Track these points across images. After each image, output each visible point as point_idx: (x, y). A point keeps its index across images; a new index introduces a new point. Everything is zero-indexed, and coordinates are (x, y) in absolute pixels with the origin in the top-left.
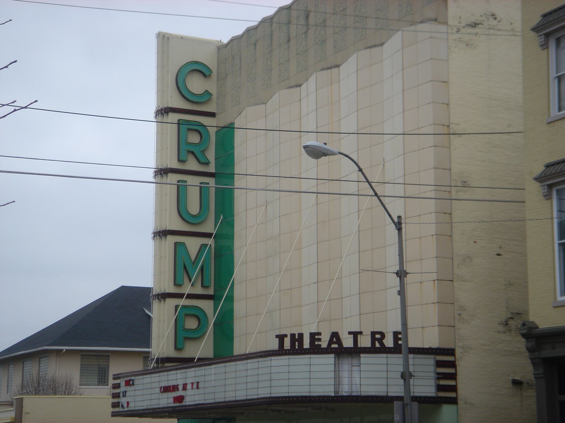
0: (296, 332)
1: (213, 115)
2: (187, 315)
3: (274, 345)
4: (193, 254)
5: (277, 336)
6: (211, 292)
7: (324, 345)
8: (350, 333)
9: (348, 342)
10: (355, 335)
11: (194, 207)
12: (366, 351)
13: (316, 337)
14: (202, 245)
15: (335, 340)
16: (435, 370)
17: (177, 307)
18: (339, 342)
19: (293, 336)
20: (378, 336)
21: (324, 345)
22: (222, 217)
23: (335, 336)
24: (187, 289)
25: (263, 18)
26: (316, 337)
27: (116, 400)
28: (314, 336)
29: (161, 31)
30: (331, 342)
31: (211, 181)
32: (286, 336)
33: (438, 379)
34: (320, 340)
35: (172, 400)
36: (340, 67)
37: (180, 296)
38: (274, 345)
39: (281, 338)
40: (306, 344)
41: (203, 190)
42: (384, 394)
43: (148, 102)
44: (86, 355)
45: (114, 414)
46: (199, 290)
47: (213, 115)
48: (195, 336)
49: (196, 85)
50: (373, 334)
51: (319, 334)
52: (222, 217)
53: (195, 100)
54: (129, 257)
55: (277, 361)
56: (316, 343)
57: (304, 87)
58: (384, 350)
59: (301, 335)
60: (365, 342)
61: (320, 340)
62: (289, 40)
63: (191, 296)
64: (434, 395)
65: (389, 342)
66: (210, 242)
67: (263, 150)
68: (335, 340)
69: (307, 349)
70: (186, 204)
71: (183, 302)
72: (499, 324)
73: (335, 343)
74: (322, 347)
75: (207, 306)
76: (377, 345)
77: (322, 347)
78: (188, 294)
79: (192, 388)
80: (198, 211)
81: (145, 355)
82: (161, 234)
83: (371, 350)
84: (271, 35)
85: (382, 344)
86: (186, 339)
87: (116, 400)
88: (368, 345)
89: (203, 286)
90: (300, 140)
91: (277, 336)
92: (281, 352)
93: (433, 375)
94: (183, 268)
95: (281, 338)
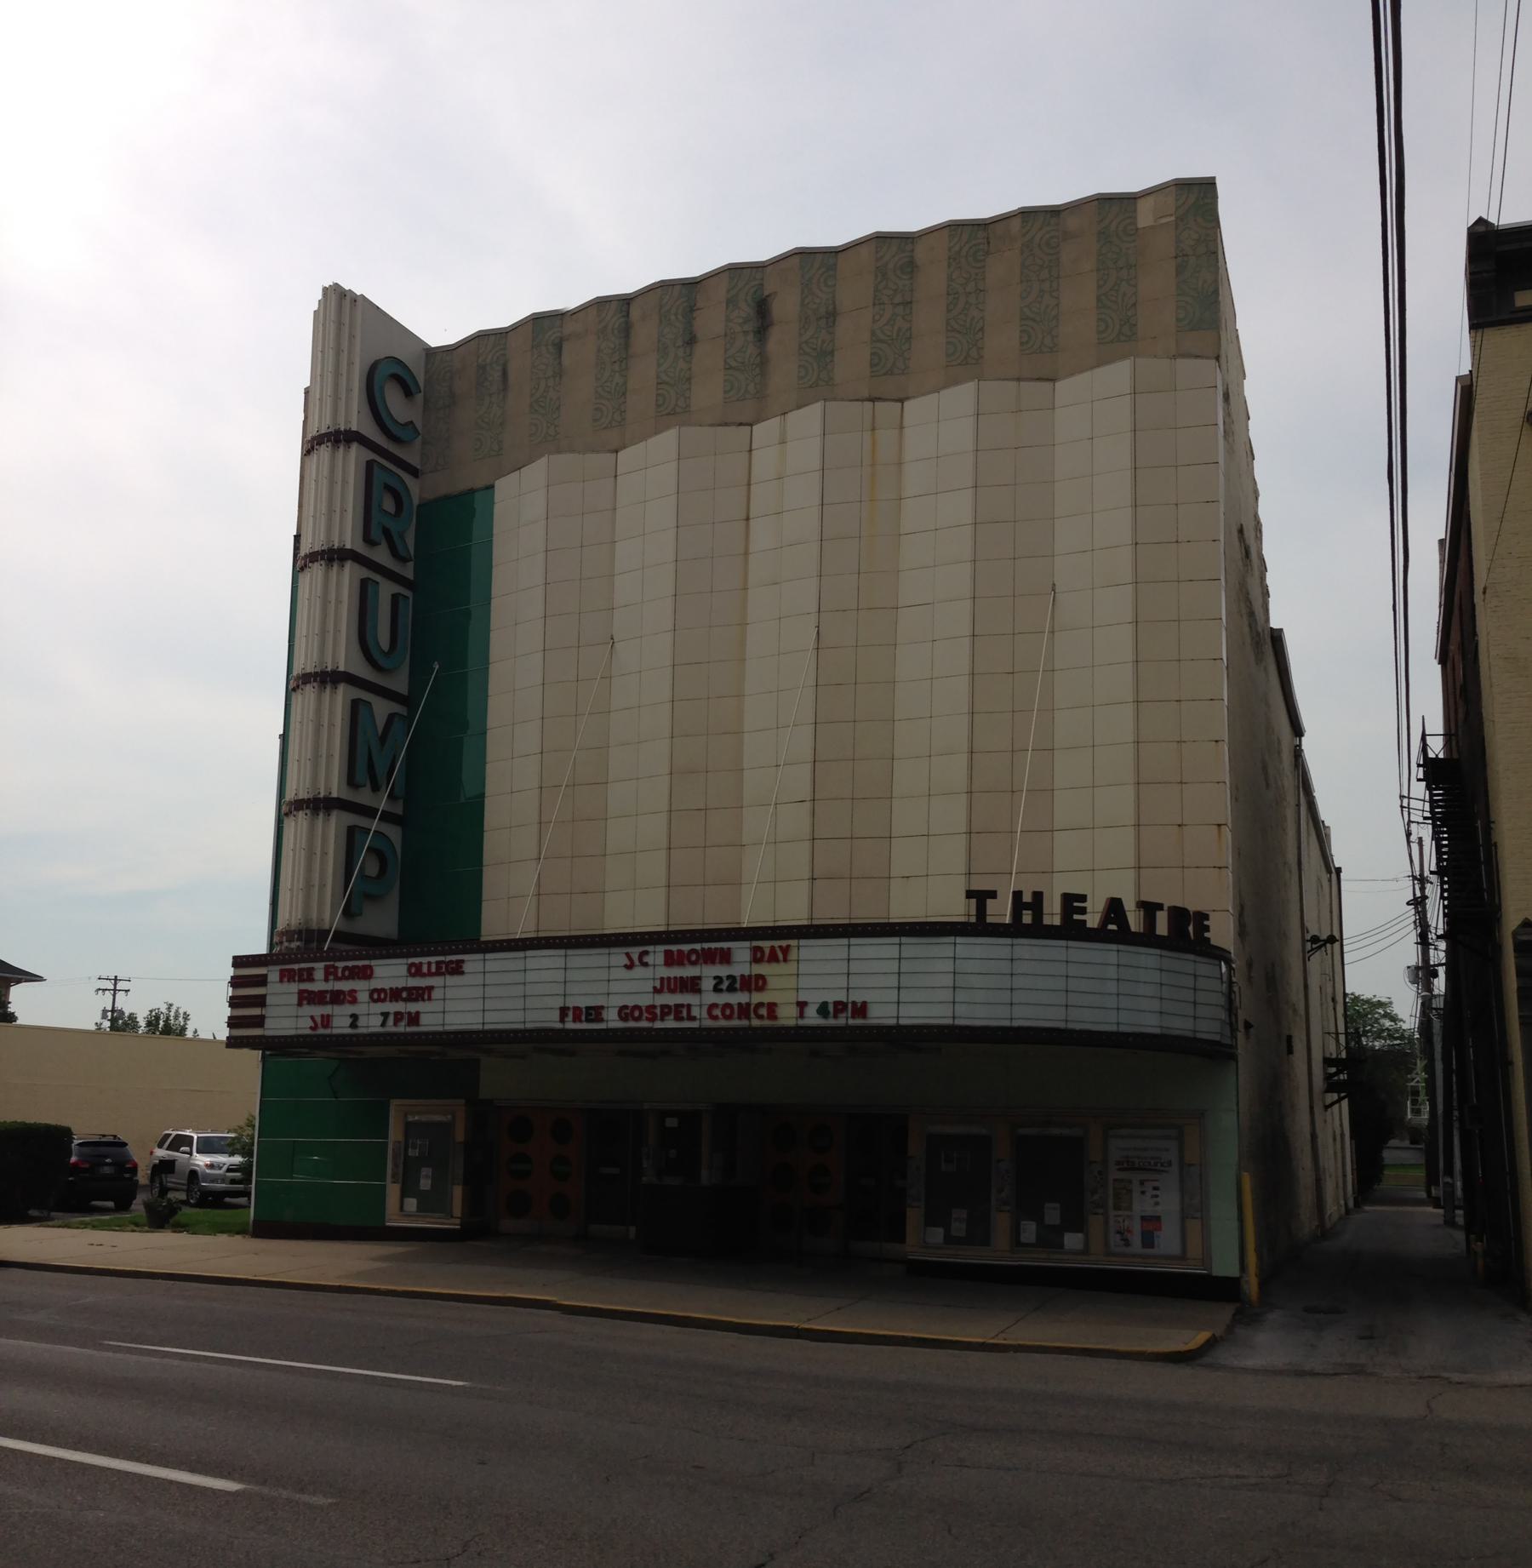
1: (414, 472)
3: (958, 909)
7: (1093, 920)
9: (1135, 921)
12: (998, 931)
21: (1093, 920)
23: (1115, 906)
29: (346, 285)
30: (1106, 920)
32: (1160, 907)
34: (1083, 911)
35: (378, 971)
36: (906, 404)
37: (369, 812)
39: (981, 897)
41: (395, 598)
47: (414, 472)
51: (1083, 898)
55: (968, 947)
56: (1076, 917)
59: (1038, 896)
60: (1000, 911)
61: (1083, 911)
62: (691, 341)
74: (1089, 925)
76: (1027, 918)
77: (1089, 925)
83: (1014, 930)
88: (1057, 921)
90: (748, 526)
92: (980, 927)
95: (981, 897)
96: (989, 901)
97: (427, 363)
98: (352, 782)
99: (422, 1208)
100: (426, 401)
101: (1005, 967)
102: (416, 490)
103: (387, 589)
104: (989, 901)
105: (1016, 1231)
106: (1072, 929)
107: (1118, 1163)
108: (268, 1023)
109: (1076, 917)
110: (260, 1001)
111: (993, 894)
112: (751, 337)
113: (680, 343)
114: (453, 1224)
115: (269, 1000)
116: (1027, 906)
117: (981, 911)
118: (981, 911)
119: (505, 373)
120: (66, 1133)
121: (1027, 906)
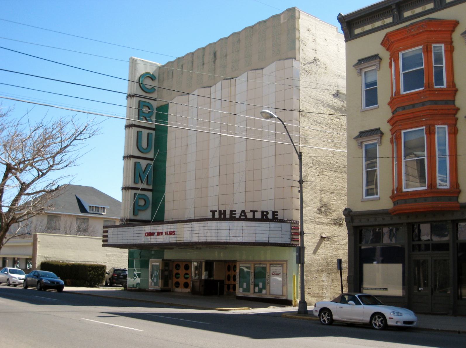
0: (222, 209)
2: (140, 198)
4: (144, 167)
5: (211, 211)
6: (151, 187)
7: (237, 216)
8: (251, 211)
9: (250, 215)
10: (254, 212)
11: (144, 144)
13: (233, 212)
14: (147, 164)
15: (243, 214)
16: (291, 231)
17: (135, 195)
18: (245, 215)
19: (220, 211)
20: (265, 213)
21: (237, 216)
22: (158, 151)
24: (140, 186)
25: (259, 22)
26: (233, 212)
27: (105, 239)
28: (232, 212)
30: (241, 215)
31: (153, 132)
33: (292, 235)
36: (263, 70)
37: (137, 189)
38: (210, 215)
39: (213, 212)
40: (228, 216)
42: (267, 242)
43: (125, 87)
44: (50, 215)
45: (104, 246)
46: (145, 186)
48: (144, 208)
49: (148, 83)
50: (263, 212)
51: (235, 211)
52: (158, 151)
53: (147, 91)
54: (27, 182)
56: (275, 217)
57: (213, 88)
58: (267, 220)
59: (225, 211)
62: (203, 64)
63: (143, 189)
64: (289, 243)
65: (270, 216)
66: (152, 163)
67: (185, 120)
68: (243, 214)
69: (217, 218)
70: (141, 143)
71: (139, 192)
72: (317, 209)
73: (243, 216)
74: (236, 217)
75: (149, 194)
77: (236, 217)
78: (141, 188)
79: (165, 235)
80: (147, 146)
81: (77, 217)
82: (127, 157)
83: (261, 220)
84: (193, 62)
85: (267, 217)
86: (139, 210)
87: (105, 239)
89: (147, 184)
90: (210, 114)
91: (211, 211)
92: (213, 219)
93: (289, 233)
94: (138, 176)
95: (213, 212)
96: (256, 213)
97: (159, 70)
98: (135, 182)
99: (155, 285)
100: (159, 80)
101: (254, 228)
102: (155, 104)
103: (145, 132)
104: (256, 213)
105: (254, 288)
106: (232, 218)
107: (272, 273)
108: (108, 241)
109: (275, 217)
110: (107, 236)
111: (257, 211)
112: (213, 63)
113: (201, 65)
114: (159, 289)
115: (108, 236)
116: (222, 214)
117: (254, 215)
118: (254, 215)
119: (173, 73)
120: (103, 268)
121: (222, 214)
